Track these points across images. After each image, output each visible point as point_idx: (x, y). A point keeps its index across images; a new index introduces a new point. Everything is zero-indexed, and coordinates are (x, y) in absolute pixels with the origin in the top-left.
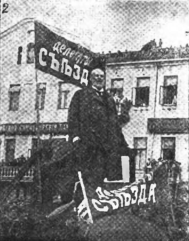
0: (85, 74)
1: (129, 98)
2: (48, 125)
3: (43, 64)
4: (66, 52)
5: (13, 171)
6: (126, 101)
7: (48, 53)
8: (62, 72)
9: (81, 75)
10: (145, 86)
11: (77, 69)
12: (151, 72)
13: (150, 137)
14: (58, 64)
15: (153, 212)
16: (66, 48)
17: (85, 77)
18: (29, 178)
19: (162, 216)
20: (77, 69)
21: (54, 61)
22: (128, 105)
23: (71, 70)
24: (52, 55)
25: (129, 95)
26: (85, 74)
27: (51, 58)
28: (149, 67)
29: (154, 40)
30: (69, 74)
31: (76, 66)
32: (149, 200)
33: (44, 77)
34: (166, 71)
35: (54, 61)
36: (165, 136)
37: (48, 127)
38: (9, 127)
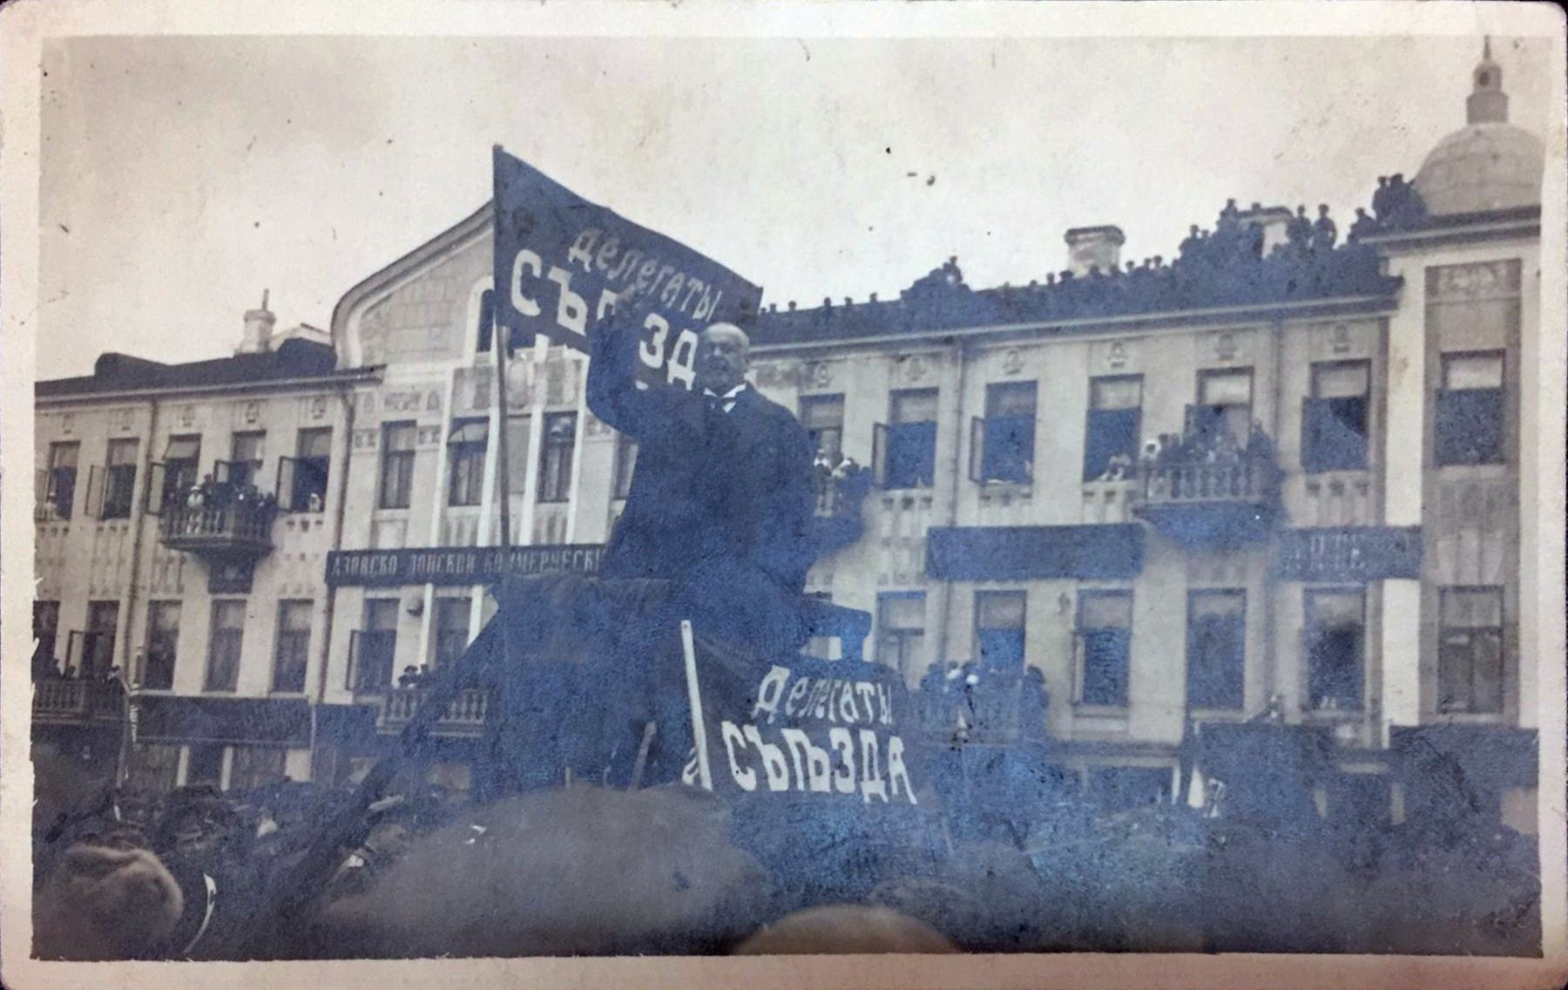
0: (686, 346)
1: (864, 460)
2: (580, 552)
6: (853, 470)
7: (545, 270)
9: (668, 354)
10: (920, 419)
11: (656, 329)
12: (941, 375)
13: (934, 592)
15: (1329, 448)
17: (682, 361)
20: (656, 329)
21: (569, 298)
22: (857, 481)
24: (558, 275)
25: (858, 448)
26: (686, 346)
27: (556, 287)
28: (935, 356)
29: (954, 259)
32: (895, 791)
34: (992, 369)
35: (569, 298)
36: (991, 586)
37: (581, 560)
38: (450, 557)
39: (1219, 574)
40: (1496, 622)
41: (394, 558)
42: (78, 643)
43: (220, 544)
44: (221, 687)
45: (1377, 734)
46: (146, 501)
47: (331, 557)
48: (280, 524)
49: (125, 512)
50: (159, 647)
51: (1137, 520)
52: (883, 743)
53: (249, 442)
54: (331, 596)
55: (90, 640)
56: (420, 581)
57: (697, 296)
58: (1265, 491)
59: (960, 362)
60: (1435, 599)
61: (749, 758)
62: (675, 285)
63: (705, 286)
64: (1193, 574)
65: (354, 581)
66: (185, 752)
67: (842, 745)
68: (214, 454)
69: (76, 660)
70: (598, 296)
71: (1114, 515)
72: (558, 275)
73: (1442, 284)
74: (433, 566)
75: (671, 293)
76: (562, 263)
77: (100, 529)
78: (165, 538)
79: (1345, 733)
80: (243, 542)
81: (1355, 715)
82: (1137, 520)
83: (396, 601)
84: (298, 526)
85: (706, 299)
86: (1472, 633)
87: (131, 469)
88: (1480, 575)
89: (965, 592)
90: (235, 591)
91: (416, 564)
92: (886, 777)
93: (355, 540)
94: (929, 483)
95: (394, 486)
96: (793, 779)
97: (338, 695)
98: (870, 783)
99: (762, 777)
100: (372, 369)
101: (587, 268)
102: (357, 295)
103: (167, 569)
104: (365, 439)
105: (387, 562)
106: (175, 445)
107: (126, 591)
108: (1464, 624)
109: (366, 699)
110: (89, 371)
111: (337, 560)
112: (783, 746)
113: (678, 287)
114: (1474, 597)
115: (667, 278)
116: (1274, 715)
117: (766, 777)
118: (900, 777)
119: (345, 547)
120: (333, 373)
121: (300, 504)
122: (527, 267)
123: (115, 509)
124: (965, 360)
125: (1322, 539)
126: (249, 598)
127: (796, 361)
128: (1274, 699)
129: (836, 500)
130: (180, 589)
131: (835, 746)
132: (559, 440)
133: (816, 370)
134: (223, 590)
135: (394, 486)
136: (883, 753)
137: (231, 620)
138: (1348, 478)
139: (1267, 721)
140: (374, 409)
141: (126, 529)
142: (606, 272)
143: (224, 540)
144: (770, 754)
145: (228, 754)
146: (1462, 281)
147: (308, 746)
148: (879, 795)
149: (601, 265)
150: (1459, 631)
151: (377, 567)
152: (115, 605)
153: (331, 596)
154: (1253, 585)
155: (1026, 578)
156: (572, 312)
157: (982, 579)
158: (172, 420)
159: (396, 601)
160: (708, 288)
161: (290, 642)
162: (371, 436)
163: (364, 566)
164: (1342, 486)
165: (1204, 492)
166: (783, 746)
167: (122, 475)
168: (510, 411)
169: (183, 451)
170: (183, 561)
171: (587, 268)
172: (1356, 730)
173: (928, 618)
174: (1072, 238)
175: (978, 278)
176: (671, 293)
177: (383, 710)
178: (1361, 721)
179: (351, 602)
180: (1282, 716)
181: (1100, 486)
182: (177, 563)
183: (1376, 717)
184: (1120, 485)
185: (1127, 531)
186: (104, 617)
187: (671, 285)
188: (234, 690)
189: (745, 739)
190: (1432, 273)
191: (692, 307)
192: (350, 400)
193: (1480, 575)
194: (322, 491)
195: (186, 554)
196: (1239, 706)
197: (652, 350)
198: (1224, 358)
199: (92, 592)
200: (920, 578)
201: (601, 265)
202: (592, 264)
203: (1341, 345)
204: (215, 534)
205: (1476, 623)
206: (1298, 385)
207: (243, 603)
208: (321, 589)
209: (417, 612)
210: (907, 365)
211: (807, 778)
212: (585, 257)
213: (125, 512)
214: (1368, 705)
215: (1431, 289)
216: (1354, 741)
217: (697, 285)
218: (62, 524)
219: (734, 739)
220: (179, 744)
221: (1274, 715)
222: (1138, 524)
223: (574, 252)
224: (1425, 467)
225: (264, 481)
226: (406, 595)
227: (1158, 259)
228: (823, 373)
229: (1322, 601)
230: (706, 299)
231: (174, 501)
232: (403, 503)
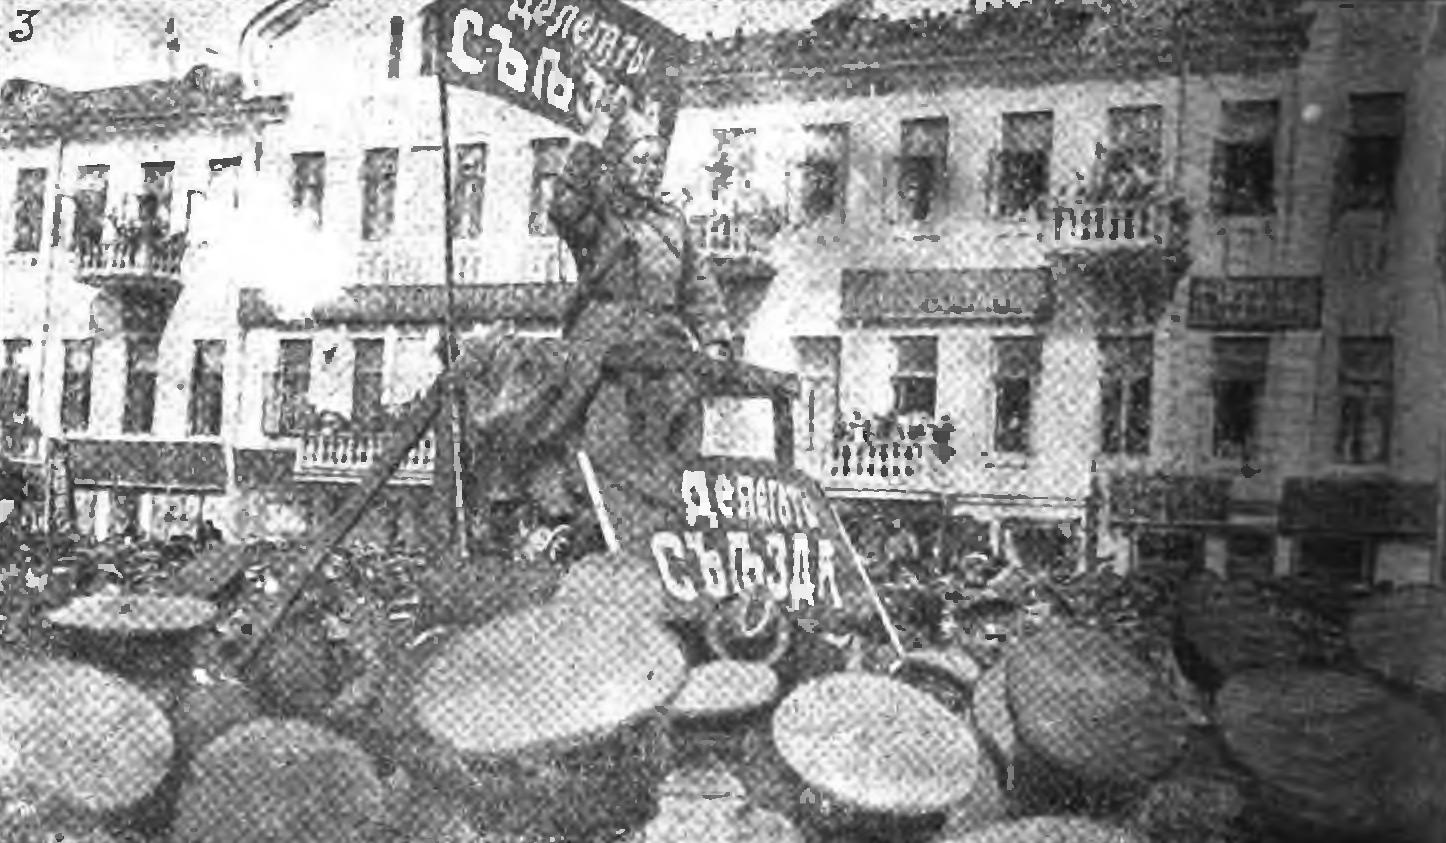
3: (471, 66)
4: (559, 20)
5: (336, 446)
7: (486, 29)
8: (537, 90)
14: (522, 66)
16: (558, 10)
18: (418, 469)
19: (1143, 468)
23: (569, 85)
24: (500, 33)
30: (562, 103)
31: (592, 75)
32: (821, 593)
33: (474, 114)
35: (509, 55)
52: (814, 546)
67: (775, 551)
88: (436, 148)
92: (814, 579)
99: (699, 585)
109: (285, 443)
118: (827, 580)
122: (668, 553)
131: (770, 552)
136: (814, 559)
144: (709, 559)
165: (1129, 234)
169: (92, 182)
186: (209, 359)
189: (687, 551)
193: (436, 148)
219: (668, 552)
227: (927, 12)
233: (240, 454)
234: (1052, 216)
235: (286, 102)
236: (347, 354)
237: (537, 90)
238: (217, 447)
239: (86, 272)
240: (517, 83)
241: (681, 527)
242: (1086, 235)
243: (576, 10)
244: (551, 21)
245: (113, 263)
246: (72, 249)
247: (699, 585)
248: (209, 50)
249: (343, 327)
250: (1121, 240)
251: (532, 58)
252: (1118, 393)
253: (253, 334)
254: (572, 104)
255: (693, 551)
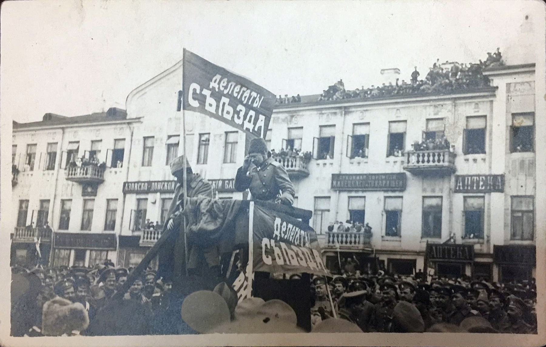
0: (251, 116)
3: (195, 104)
7: (201, 90)
9: (245, 119)
11: (241, 110)
12: (337, 120)
13: (334, 196)
14: (214, 103)
17: (250, 121)
20: (241, 110)
21: (210, 100)
22: (308, 158)
24: (206, 92)
26: (251, 116)
27: (205, 97)
28: (335, 113)
30: (229, 117)
34: (355, 117)
35: (210, 100)
36: (353, 194)
38: (166, 184)
39: (433, 191)
40: (531, 208)
41: (146, 184)
42: (36, 214)
43: (86, 180)
44: (86, 229)
45: (489, 248)
46: (60, 165)
47: (125, 184)
48: (107, 171)
49: (53, 168)
50: (64, 215)
51: (405, 171)
53: (97, 143)
54: (125, 197)
55: (40, 212)
56: (155, 192)
57: (255, 99)
58: (450, 162)
59: (343, 115)
60: (509, 199)
61: (270, 252)
62: (247, 94)
63: (257, 95)
64: (424, 190)
65: (131, 192)
66: (73, 253)
68: (84, 148)
69: (35, 220)
70: (220, 99)
71: (397, 169)
72: (206, 92)
73: (512, 89)
74: (160, 187)
75: (245, 97)
76: (208, 88)
77: (44, 174)
78: (67, 177)
79: (477, 247)
80: (93, 178)
81: (481, 241)
82: (405, 171)
83: (147, 199)
84: (113, 173)
85: (258, 99)
86: (523, 212)
87: (55, 153)
89: (345, 196)
90: (91, 196)
91: (154, 186)
93: (133, 178)
94: (332, 157)
95: (146, 159)
96: (285, 261)
97: (126, 232)
98: (214, 83)
99: (274, 259)
100: (140, 118)
101: (217, 90)
102: (135, 92)
103: (67, 188)
104: (137, 142)
105: (144, 186)
106: (71, 144)
107: (53, 196)
108: (519, 209)
109: (136, 234)
110: (41, 119)
111: (127, 185)
112: (280, 248)
113: (248, 95)
114: (523, 199)
115: (244, 92)
116: (452, 240)
117: (275, 259)
119: (129, 181)
120: (126, 119)
121: (114, 165)
123: (51, 167)
124: (345, 114)
125: (470, 178)
126: (96, 198)
127: (286, 115)
128: (452, 235)
129: (300, 164)
130: (72, 195)
132: (204, 143)
133: (293, 119)
134: (87, 195)
135: (146, 159)
137: (89, 206)
138: (479, 156)
139: (449, 243)
140: (140, 132)
141: (53, 174)
142: (223, 91)
143: (87, 178)
144: (277, 251)
145: (88, 253)
146: (518, 87)
147: (115, 250)
148: (215, 88)
149: (222, 89)
150: (519, 211)
151: (140, 187)
152: (48, 201)
153: (125, 197)
154: (445, 195)
155: (366, 191)
156: (210, 105)
157: (350, 191)
158: (70, 135)
159: (147, 199)
160: (259, 95)
161: (110, 212)
162: (139, 141)
163: (136, 187)
164: (476, 160)
166: (280, 248)
167: (52, 156)
168: (187, 132)
169: (74, 147)
170: (73, 185)
171: (217, 90)
172: (481, 246)
173: (331, 204)
174: (382, 72)
175: (350, 87)
176: (245, 97)
177: (142, 237)
178: (483, 243)
179: (132, 199)
180: (455, 241)
181: (392, 158)
182: (71, 186)
183: (488, 241)
184: (400, 159)
185: (401, 176)
186: (45, 205)
187: (245, 95)
188: (90, 230)
190: (508, 85)
191: (253, 102)
192: (132, 129)
194: (122, 160)
195: (74, 183)
196: (439, 236)
197: (239, 118)
198: (435, 114)
199: (41, 196)
200: (329, 192)
201: (222, 89)
202: (219, 88)
203: (476, 110)
204: (85, 176)
205: (524, 208)
206: (462, 124)
207: (94, 200)
208: (120, 196)
209: (154, 203)
210: (325, 116)
211: (289, 260)
212: (216, 86)
213: (53, 168)
214: (486, 237)
215: (508, 91)
216: (481, 250)
217: (254, 94)
218: (31, 173)
220: (70, 250)
221: (452, 240)
222: (405, 173)
223: (212, 84)
224: (506, 153)
225: (101, 158)
226: (151, 197)
228: (296, 119)
229: (471, 201)
230: (258, 99)
231: (71, 165)
232: (149, 164)
233: (121, 237)
234: (406, 155)
235: (142, 120)
236: (159, 203)
237: (220, 114)
238: (114, 235)
239: (70, 176)
240: (213, 110)
241: (270, 237)
242: (418, 162)
243: (234, 84)
244: (226, 88)
245: (79, 173)
246: (66, 169)
247: (274, 259)
248: (116, 103)
249: (158, 194)
250: (436, 163)
251: (218, 101)
252: (240, 138)
253: (128, 196)
254: (233, 117)
255: (272, 247)
